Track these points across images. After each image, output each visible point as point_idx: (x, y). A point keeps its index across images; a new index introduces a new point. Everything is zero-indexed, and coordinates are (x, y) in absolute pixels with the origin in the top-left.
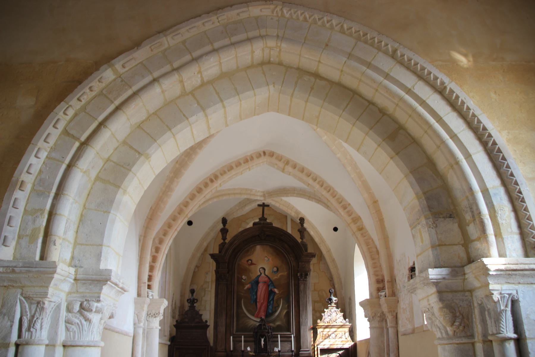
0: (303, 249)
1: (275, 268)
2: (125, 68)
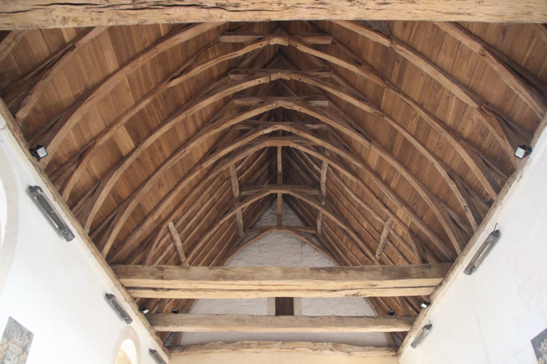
0: (233, 235)
1: (41, 155)
2: (431, 325)
